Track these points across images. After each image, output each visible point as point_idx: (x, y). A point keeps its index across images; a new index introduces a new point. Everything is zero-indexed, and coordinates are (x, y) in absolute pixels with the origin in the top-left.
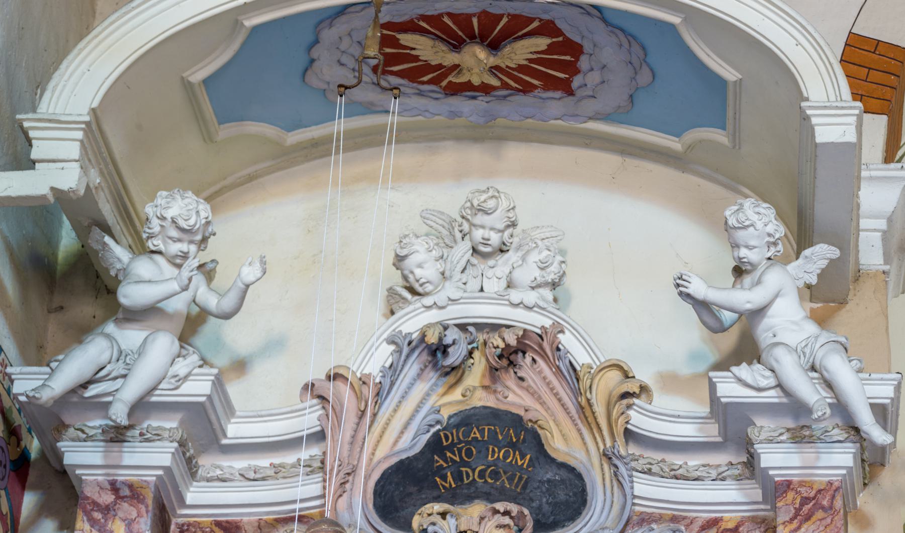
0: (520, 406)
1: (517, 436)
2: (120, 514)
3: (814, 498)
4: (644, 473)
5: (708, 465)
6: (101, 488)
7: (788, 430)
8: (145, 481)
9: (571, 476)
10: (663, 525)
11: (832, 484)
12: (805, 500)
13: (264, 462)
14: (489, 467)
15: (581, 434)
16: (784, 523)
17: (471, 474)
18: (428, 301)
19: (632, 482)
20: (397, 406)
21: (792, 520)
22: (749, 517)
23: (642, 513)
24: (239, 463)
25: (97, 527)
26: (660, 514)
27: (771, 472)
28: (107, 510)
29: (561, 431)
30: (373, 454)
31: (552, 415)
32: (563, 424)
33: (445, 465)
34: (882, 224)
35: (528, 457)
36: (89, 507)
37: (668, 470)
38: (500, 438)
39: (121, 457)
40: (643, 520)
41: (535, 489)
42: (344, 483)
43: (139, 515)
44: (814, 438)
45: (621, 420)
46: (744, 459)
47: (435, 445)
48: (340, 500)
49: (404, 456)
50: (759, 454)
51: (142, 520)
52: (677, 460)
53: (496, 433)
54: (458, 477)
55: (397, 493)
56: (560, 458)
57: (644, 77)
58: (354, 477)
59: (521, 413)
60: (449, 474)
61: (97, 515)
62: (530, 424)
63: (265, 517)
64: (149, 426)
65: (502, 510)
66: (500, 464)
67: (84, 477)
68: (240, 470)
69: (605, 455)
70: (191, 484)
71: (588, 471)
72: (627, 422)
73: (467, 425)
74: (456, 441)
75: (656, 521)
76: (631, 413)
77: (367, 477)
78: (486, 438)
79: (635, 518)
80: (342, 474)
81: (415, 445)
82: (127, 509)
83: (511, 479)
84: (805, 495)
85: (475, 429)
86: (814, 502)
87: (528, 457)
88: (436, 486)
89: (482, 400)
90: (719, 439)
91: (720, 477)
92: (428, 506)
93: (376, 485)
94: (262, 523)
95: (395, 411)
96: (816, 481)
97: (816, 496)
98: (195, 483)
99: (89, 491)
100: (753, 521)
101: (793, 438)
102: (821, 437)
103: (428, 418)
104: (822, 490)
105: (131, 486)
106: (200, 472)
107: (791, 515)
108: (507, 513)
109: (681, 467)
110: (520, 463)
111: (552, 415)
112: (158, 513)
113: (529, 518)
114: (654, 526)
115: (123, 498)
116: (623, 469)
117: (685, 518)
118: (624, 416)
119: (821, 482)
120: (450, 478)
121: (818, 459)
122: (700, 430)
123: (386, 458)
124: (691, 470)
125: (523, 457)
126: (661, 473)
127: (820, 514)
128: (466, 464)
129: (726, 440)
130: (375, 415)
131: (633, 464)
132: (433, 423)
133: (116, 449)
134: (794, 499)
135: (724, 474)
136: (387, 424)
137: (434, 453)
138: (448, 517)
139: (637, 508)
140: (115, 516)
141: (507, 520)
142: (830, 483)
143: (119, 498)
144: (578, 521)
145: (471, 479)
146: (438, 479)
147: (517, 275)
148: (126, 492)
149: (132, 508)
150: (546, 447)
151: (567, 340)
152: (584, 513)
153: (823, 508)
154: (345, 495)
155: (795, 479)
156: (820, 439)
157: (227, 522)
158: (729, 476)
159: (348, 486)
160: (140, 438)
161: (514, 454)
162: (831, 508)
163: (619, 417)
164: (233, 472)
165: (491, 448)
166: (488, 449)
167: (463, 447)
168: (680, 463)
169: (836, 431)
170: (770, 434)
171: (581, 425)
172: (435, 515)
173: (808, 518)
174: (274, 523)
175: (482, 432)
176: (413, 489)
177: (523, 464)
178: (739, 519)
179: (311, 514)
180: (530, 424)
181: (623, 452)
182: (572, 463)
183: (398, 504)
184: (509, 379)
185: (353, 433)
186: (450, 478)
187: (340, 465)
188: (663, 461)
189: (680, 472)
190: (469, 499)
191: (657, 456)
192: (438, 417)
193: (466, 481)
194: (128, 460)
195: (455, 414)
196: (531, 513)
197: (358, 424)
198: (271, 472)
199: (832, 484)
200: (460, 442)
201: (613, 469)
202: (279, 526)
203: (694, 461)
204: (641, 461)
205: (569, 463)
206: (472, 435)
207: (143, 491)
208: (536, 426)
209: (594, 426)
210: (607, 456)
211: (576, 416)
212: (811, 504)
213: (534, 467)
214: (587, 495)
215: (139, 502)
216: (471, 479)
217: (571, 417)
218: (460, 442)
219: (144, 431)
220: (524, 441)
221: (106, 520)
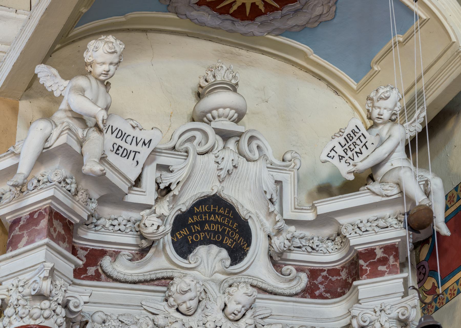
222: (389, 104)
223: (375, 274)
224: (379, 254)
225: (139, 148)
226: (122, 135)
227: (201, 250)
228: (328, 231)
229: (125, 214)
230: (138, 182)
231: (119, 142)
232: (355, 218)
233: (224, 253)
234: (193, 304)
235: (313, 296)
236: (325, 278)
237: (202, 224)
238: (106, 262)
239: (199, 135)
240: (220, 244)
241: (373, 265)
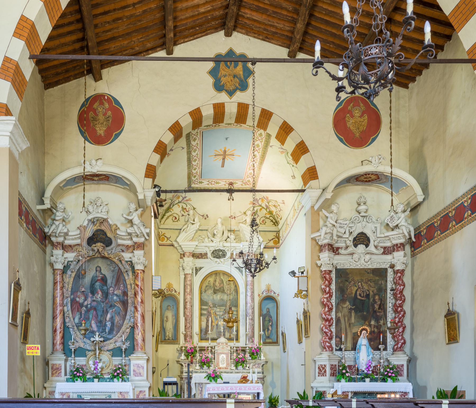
12: (138, 245)
13: (73, 237)
18: (91, 214)
24: (71, 237)
34: (151, 198)
47: (94, 235)
52: (123, 237)
54: (97, 239)
57: (118, 180)
82: (59, 246)
89: (99, 228)
99: (54, 243)
147: (102, 211)
151: (109, 220)
184: (102, 224)
191: (121, 237)
203: (125, 237)
222: (401, 209)
223: (398, 251)
224: (399, 245)
225: (344, 226)
226: (341, 224)
227: (359, 246)
228: (387, 238)
229: (343, 239)
230: (345, 233)
231: (340, 225)
232: (393, 236)
233: (364, 246)
234: (358, 260)
235: (385, 254)
236: (388, 249)
237: (359, 239)
238: (340, 250)
239: (357, 218)
240: (363, 244)
241: (397, 248)
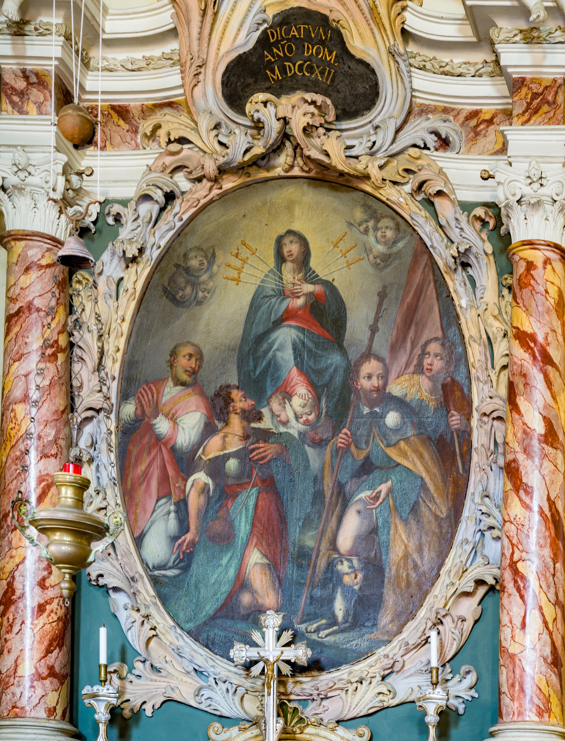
0: (326, 7)
1: (325, 34)
2: (32, 98)
3: (541, 94)
4: (420, 69)
5: (469, 63)
6: (16, 76)
7: (521, 31)
8: (47, 70)
9: (367, 71)
10: (437, 115)
11: (556, 81)
12: (535, 96)
14: (305, 62)
15: (373, 33)
16: (518, 116)
17: (293, 68)
19: (410, 77)
20: (234, 6)
21: (524, 113)
22: (501, 110)
23: (421, 104)
25: (17, 109)
26: (435, 106)
27: (509, 70)
28: (22, 94)
29: (358, 30)
30: (219, 49)
31: (351, 15)
32: (360, 24)
33: (273, 60)
35: (334, 53)
36: (9, 92)
37: (438, 67)
38: (313, 36)
39: (25, 48)
40: (422, 111)
41: (341, 82)
42: (197, 74)
43: (45, 99)
44: (541, 39)
45: (398, 21)
46: (494, 58)
48: (196, 89)
49: (241, 52)
50: (499, 53)
51: (48, 103)
52: (444, 57)
53: (310, 31)
54: (283, 70)
55: (239, 83)
56: (358, 55)
58: (205, 69)
59: (327, 13)
60: (276, 68)
61: (16, 99)
62: (334, 24)
63: (146, 103)
64: (41, 21)
65: (310, 101)
66: (314, 60)
67: (2, 66)
68: (121, 61)
69: (390, 53)
70: (87, 74)
71: (379, 67)
72: (403, 23)
73: (288, 24)
74: (279, 38)
75: (431, 112)
76: (406, 14)
77: (215, 70)
78: (302, 36)
79: (416, 109)
80: (194, 67)
81: (248, 41)
82: (36, 94)
83: (322, 73)
84: (535, 91)
85: (294, 28)
86: (541, 97)
87: (334, 53)
88: (267, 78)
90: (474, 39)
91: (477, 73)
92: (255, 95)
93: (223, 77)
94: (144, 107)
95: (232, 10)
96: (544, 79)
97: (543, 91)
98: (90, 73)
99: (8, 78)
100: (504, 114)
101: (524, 39)
102: (547, 38)
103: (257, 17)
104: (548, 87)
105: (37, 74)
106: (91, 62)
107: (524, 108)
108: (313, 103)
109: (447, 64)
110: (328, 59)
111: (351, 15)
112: (62, 98)
113: (331, 106)
114: (430, 116)
115: (32, 84)
116: (402, 66)
117: (453, 110)
118: (400, 17)
119: (547, 80)
120: (277, 71)
121: (544, 58)
122: (460, 31)
123: (228, 52)
124: (455, 67)
125: (330, 53)
126: (433, 69)
127: (545, 108)
128: (289, 59)
129: (480, 40)
130: (216, 14)
131: (412, 61)
132: (261, 22)
133: (20, 42)
134: (527, 94)
135: (480, 71)
136: (227, 22)
137: (264, 48)
138: (268, 105)
139: (418, 101)
140: (28, 99)
141: (312, 109)
142: (555, 81)
143: (30, 84)
144: (373, 111)
145: (293, 72)
146: (268, 72)
148: (34, 79)
149: (40, 93)
150: (347, 45)
152: (377, 104)
153: (548, 103)
154: (199, 84)
155: (528, 76)
156: (546, 40)
157: (119, 106)
158: (485, 73)
159: (201, 77)
160: (35, 33)
161: (324, 51)
162: (554, 103)
163: (396, 18)
164: (116, 63)
165: (306, 44)
166: (304, 46)
167: (285, 44)
168: (447, 60)
169: (559, 33)
170: (507, 35)
171: (373, 25)
172: (259, 103)
173: (536, 111)
174: (153, 107)
175: (299, 30)
176: (250, 80)
177: (331, 60)
178: (494, 112)
179: (179, 101)
180: (334, 24)
181: (402, 50)
182: (367, 59)
183: (241, 94)
185: (199, 30)
186: (277, 71)
187: (192, 59)
188: (434, 58)
189: (447, 68)
190: (292, 90)
191: (429, 53)
192: (264, 16)
193: (289, 75)
194: (31, 51)
195: (278, 14)
196: (332, 103)
197: (202, 22)
198: (143, 64)
199: (556, 81)
200: (283, 39)
201: (396, 64)
202: (157, 110)
204: (418, 58)
205: (365, 59)
206: (292, 33)
207: (46, 79)
208: (339, 26)
209: (380, 26)
210: (392, 54)
211: (369, 17)
212: (539, 99)
213: (339, 63)
214: (379, 88)
215: (44, 88)
216: (293, 72)
217: (365, 18)
218: (283, 39)
219: (38, 27)
220: (331, 39)
221: (22, 103)
